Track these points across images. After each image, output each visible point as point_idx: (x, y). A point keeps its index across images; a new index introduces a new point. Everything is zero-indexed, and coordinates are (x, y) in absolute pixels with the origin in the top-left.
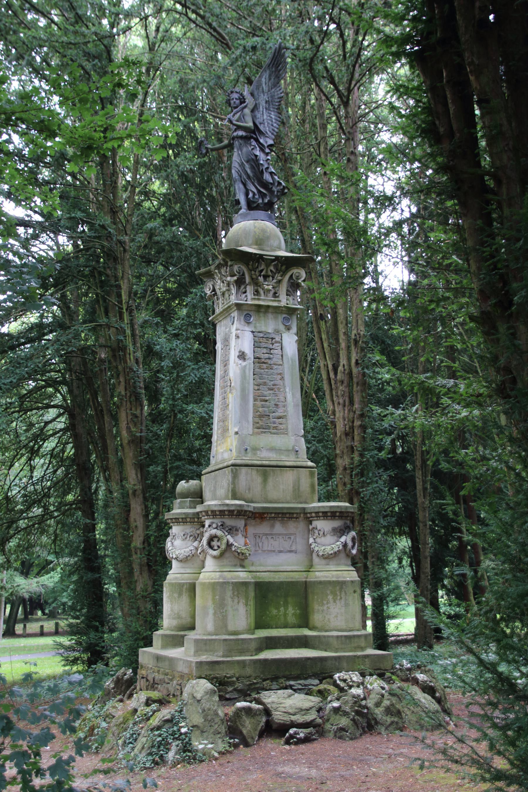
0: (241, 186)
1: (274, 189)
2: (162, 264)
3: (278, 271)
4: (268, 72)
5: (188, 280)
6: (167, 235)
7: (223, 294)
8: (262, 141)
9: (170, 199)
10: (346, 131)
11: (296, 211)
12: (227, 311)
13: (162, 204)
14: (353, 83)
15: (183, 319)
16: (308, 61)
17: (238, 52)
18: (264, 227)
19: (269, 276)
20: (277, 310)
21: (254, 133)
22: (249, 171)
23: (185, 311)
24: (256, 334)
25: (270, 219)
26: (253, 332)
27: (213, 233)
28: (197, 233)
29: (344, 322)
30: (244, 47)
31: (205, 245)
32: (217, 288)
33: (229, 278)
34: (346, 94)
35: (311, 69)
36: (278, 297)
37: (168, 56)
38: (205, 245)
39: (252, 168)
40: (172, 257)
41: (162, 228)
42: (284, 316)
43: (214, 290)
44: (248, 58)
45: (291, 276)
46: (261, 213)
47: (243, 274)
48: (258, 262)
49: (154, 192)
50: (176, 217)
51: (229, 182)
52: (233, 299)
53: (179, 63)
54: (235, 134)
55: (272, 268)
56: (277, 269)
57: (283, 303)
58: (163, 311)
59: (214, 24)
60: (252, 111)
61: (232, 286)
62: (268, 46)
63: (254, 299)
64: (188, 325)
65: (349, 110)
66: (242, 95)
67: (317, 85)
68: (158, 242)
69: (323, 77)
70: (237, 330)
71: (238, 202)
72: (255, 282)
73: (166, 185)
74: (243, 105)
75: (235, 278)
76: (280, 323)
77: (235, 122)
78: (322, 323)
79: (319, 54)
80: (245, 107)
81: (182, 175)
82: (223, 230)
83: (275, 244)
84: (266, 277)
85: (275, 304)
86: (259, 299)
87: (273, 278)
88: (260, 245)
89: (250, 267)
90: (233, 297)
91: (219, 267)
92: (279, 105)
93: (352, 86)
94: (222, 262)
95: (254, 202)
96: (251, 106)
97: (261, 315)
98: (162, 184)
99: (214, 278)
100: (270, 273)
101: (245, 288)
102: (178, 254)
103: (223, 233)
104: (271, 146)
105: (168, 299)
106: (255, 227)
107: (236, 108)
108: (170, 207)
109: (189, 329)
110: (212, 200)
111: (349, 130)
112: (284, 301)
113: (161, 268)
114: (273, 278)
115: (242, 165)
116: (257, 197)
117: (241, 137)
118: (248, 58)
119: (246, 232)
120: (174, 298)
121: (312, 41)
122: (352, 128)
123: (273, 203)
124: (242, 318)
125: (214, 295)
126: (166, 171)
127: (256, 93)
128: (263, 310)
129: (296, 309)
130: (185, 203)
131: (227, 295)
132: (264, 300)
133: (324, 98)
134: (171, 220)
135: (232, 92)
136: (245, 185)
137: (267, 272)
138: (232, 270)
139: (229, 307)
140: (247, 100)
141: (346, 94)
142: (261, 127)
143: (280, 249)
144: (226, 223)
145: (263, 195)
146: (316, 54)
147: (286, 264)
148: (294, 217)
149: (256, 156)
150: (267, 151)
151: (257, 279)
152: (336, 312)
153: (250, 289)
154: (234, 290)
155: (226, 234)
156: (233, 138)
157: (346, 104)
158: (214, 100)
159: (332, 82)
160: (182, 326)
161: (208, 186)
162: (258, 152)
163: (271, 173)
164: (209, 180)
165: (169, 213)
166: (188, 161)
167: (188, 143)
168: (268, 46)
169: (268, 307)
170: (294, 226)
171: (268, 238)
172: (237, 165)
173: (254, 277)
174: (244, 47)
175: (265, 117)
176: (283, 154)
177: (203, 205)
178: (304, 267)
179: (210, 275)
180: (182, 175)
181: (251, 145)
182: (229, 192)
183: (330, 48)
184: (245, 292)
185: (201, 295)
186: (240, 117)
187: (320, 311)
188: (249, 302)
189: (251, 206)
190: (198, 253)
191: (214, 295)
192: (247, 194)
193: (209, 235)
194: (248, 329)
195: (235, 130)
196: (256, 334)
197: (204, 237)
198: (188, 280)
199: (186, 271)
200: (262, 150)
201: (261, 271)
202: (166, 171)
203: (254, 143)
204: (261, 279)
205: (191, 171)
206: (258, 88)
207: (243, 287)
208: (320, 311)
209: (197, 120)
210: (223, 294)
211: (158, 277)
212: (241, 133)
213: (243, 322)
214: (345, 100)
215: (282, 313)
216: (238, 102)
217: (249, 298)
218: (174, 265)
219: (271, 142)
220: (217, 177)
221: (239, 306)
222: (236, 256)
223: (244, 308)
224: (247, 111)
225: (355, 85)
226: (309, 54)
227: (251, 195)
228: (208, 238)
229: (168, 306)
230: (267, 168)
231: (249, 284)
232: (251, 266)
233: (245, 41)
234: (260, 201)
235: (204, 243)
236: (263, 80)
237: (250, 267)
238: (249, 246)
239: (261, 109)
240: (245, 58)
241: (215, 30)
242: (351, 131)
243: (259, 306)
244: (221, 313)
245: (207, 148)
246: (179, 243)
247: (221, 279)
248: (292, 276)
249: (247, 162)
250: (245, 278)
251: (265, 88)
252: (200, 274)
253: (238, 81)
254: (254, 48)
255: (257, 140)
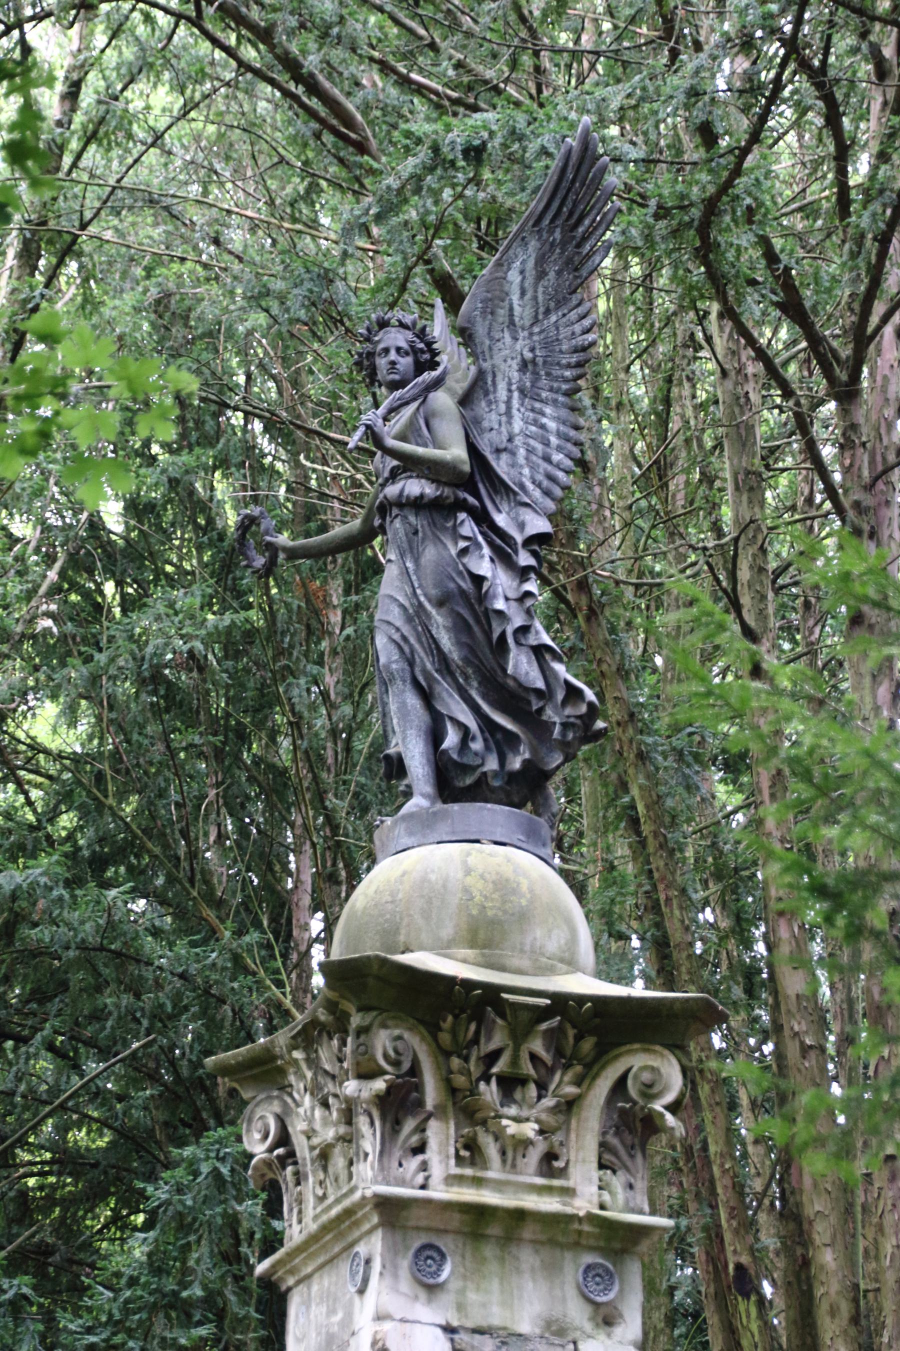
0: (413, 701)
1: (551, 714)
2: (51, 1047)
3: (563, 1058)
4: (533, 244)
5: (161, 1116)
6: (82, 920)
7: (324, 1156)
8: (501, 520)
9: (100, 777)
10: (846, 503)
11: (634, 823)
12: (340, 1229)
13: (64, 798)
14: (879, 309)
15: (133, 1282)
16: (696, 213)
17: (410, 165)
18: (507, 871)
19: (523, 1081)
20: (558, 1233)
21: (470, 488)
22: (446, 641)
23: (138, 1250)
24: (462, 1338)
25: (530, 840)
26: (449, 1330)
27: (274, 920)
28: (210, 914)
29: (845, 1308)
30: (436, 149)
31: (239, 965)
32: (297, 1127)
33: (351, 1087)
34: (846, 352)
35: (706, 251)
36: (562, 1173)
37: (110, 204)
38: (239, 965)
39: (460, 627)
40: (98, 1016)
41: (60, 891)
42: (589, 1258)
43: (284, 1139)
44: (447, 194)
45: (620, 1084)
46: (494, 815)
47: (415, 1070)
48: (479, 1017)
49: (36, 748)
50: (119, 854)
51: (347, 709)
52: (368, 1180)
53: (157, 233)
54: (392, 490)
55: (537, 1045)
56: (559, 1053)
57: (584, 1203)
58: (45, 1251)
59: (312, 62)
60: (465, 401)
61: (362, 1122)
62: (533, 147)
63: (459, 1180)
64: (153, 1308)
65: (859, 415)
66: (422, 334)
67: (729, 313)
68: (37, 953)
69: (753, 283)
70: (380, 1317)
71: (396, 768)
72: (464, 1108)
73: (83, 727)
74: (428, 376)
75: (380, 1085)
76: (571, 1293)
77: (391, 442)
78: (746, 1309)
79: (742, 182)
80: (437, 383)
81: (152, 679)
82: (317, 906)
83: (554, 944)
84: (510, 1085)
85: (550, 1204)
86: (478, 1182)
87: (542, 1087)
88: (488, 944)
89: (445, 1038)
90: (365, 1170)
91: (308, 1037)
92: (571, 376)
93: (874, 320)
94: (323, 1016)
95: (466, 769)
96: (459, 383)
97: (489, 1251)
98: (71, 716)
99: (285, 1088)
100: (528, 1069)
101: (421, 1129)
102: (126, 999)
103: (316, 925)
104: (541, 539)
105: (68, 1203)
106: (468, 872)
107: (394, 386)
108: (100, 807)
109: (158, 1329)
110: (276, 785)
111: (857, 495)
112: (587, 1190)
113: (44, 1064)
114: (542, 1087)
115: (416, 616)
116: (477, 745)
117: (418, 504)
118: (447, 194)
119: (431, 896)
120: (94, 1197)
121: (707, 134)
122: (870, 488)
123: (547, 775)
124: (405, 1264)
125: (283, 1161)
126: (88, 659)
127: (480, 330)
128: (495, 1230)
129: (642, 1231)
130: (162, 794)
131: (338, 1162)
132: (499, 1186)
133: (754, 368)
134: (99, 863)
135: (383, 324)
136: (427, 696)
137: (515, 1061)
138: (364, 1051)
139: (348, 1213)
140: (443, 358)
141: (846, 352)
142: (501, 467)
143: (571, 964)
144: (333, 879)
145: (500, 742)
146: (729, 184)
147: (603, 1027)
148: (622, 850)
149: (478, 580)
150: (525, 559)
151: (473, 1091)
152: (806, 1263)
153: (441, 1137)
154: (370, 1141)
155: (329, 928)
156: (384, 509)
157: (847, 394)
158: (295, 383)
159: (793, 308)
160: (126, 1311)
161: (259, 725)
162: (483, 564)
163: (539, 651)
164: (265, 702)
165: (90, 832)
166: (176, 623)
167: (183, 554)
168: (533, 147)
169: (520, 1215)
170: (622, 883)
171: (523, 917)
172: (396, 616)
173: (460, 1081)
174: (436, 149)
175: (518, 425)
176: (583, 586)
177: (236, 805)
178: (678, 1047)
179: (267, 1072)
180: (152, 679)
181: (456, 536)
182: (348, 749)
183: (788, 156)
184: (420, 1149)
185: (216, 1173)
186: (412, 422)
187: (735, 1254)
188: (439, 1192)
189: (454, 783)
190: (209, 999)
191: (283, 1161)
192: (435, 736)
193: (258, 925)
194: (430, 1314)
195: (394, 475)
196: (462, 1338)
197: (239, 933)
198: (161, 1116)
199: (154, 1077)
200: (503, 555)
201: (493, 1057)
202: (88, 659)
203: (468, 527)
204: (490, 1092)
205: (194, 662)
206: (490, 307)
207: (409, 1125)
208: (735, 1254)
209: (223, 463)
210: (324, 1156)
211: (34, 1099)
212: (414, 487)
213: (406, 1284)
214: (844, 376)
215: (577, 1245)
216: (406, 363)
217: (436, 1175)
218: (104, 1053)
219: (539, 525)
220: (300, 691)
221: (391, 1210)
222: (380, 987)
223: (415, 1217)
224: (443, 400)
225: (885, 319)
226: (702, 184)
227: (451, 739)
228: (252, 937)
229: (67, 1229)
230: (524, 630)
231: (439, 1112)
232: (450, 1033)
233: (439, 126)
234: (492, 764)
235: (236, 959)
236: (514, 276)
237: (445, 1038)
238: (442, 948)
239: (502, 394)
240: (436, 195)
241: (313, 88)
242: (868, 500)
243: (480, 1214)
244: (313, 1239)
245: (272, 549)
246: (127, 957)
247: (315, 1089)
248: (621, 1082)
249: (440, 603)
250: (419, 1087)
251: (522, 310)
252: (225, 1070)
253: (403, 288)
254: (475, 154)
255: (482, 518)
